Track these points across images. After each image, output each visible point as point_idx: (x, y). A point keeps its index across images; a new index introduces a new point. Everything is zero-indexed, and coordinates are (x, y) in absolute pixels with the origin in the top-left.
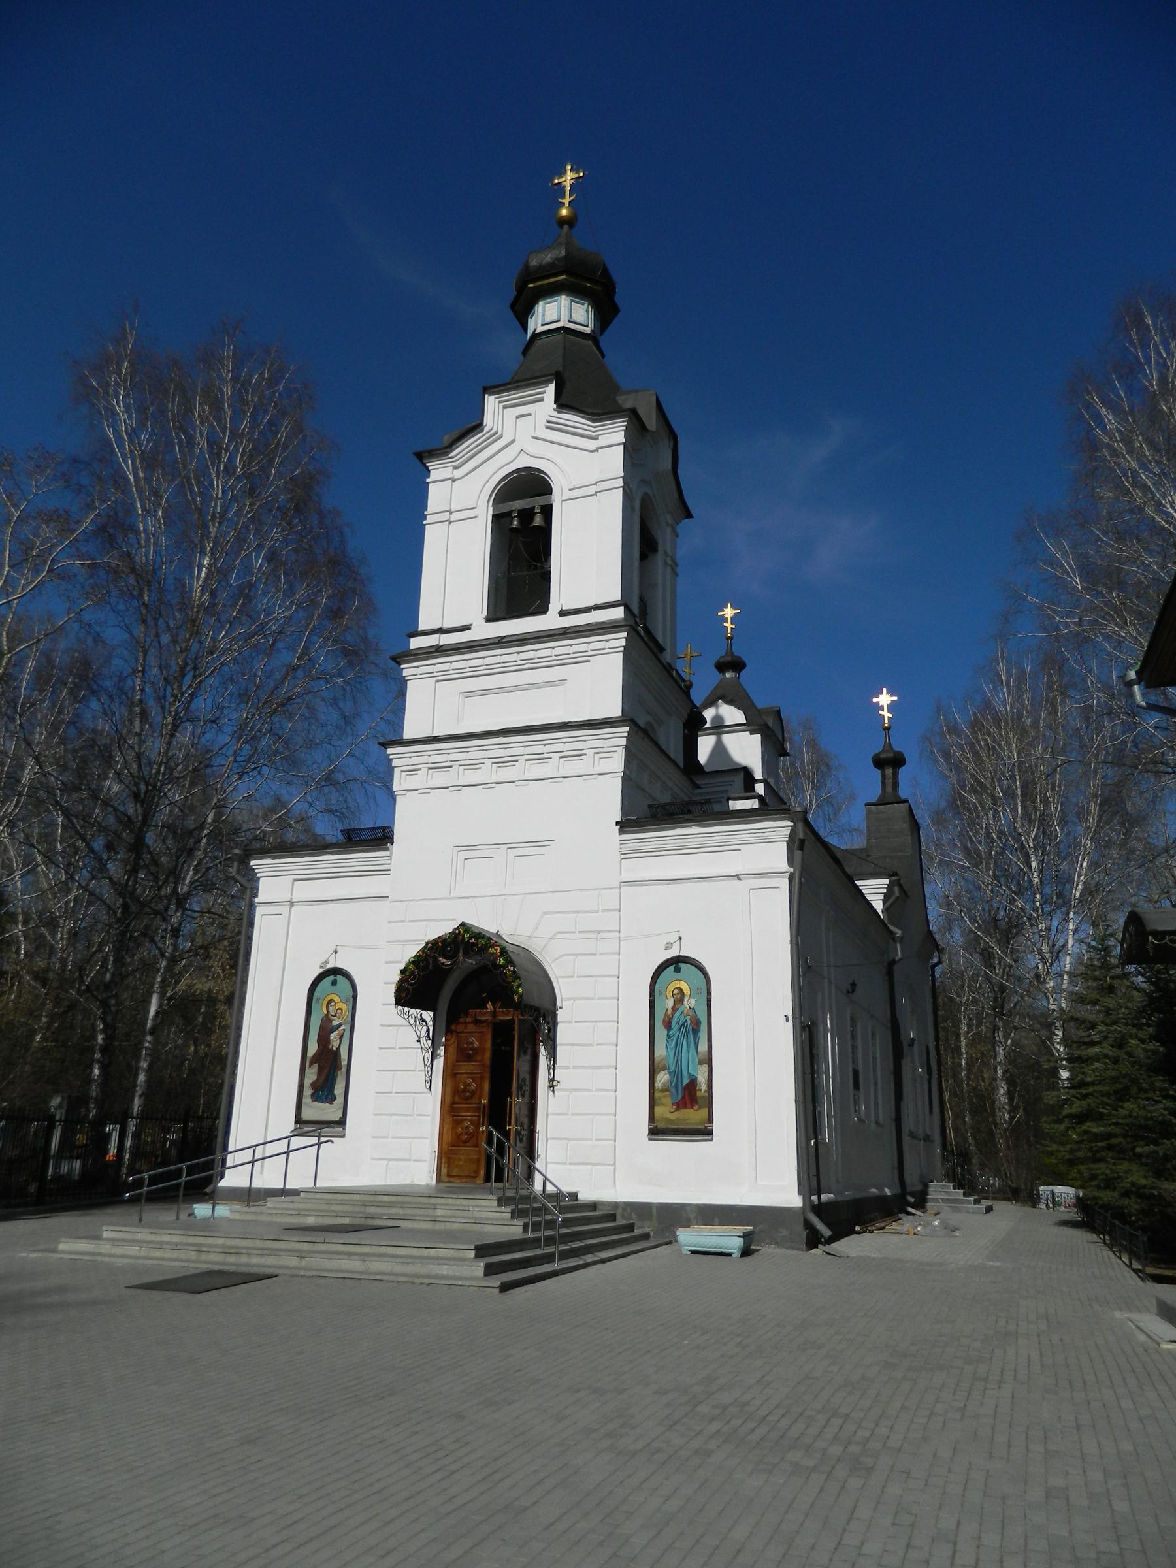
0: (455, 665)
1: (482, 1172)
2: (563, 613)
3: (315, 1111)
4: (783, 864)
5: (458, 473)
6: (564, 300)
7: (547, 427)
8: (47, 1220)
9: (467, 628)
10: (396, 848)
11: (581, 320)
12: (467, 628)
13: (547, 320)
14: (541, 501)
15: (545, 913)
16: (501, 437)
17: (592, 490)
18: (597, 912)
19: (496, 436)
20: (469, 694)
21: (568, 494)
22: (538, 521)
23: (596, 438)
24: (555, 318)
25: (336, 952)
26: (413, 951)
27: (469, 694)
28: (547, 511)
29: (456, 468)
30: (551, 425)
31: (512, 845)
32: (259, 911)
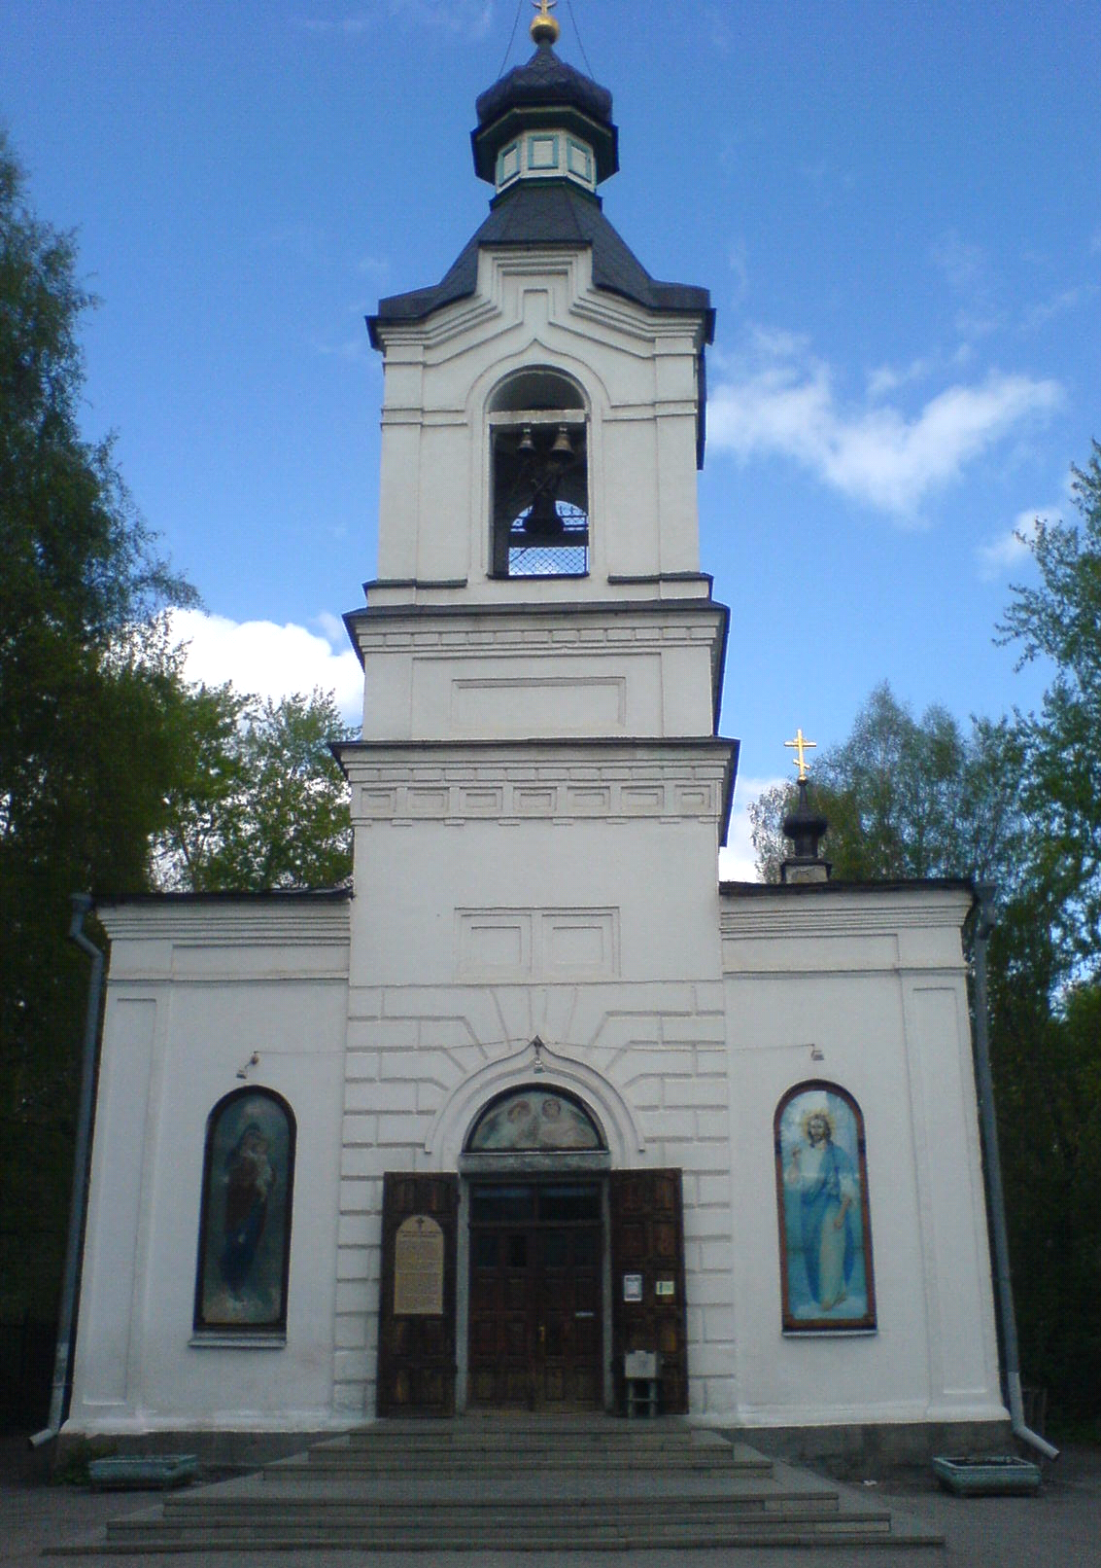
0: (446, 639)
1: (727, 1346)
3: (232, 1307)
4: (958, 959)
5: (432, 357)
6: (562, 137)
7: (572, 313)
8: (255, 1359)
9: (461, 585)
10: (357, 908)
11: (582, 171)
12: (461, 585)
13: (538, 163)
14: (571, 416)
15: (611, 1014)
16: (499, 315)
17: (649, 413)
18: (688, 1014)
19: (493, 314)
20: (465, 684)
21: (610, 414)
22: (562, 444)
23: (652, 340)
24: (549, 162)
25: (254, 1062)
26: (221, 1096)
27: (465, 684)
28: (578, 434)
29: (427, 348)
30: (578, 312)
31: (550, 912)
32: (112, 994)
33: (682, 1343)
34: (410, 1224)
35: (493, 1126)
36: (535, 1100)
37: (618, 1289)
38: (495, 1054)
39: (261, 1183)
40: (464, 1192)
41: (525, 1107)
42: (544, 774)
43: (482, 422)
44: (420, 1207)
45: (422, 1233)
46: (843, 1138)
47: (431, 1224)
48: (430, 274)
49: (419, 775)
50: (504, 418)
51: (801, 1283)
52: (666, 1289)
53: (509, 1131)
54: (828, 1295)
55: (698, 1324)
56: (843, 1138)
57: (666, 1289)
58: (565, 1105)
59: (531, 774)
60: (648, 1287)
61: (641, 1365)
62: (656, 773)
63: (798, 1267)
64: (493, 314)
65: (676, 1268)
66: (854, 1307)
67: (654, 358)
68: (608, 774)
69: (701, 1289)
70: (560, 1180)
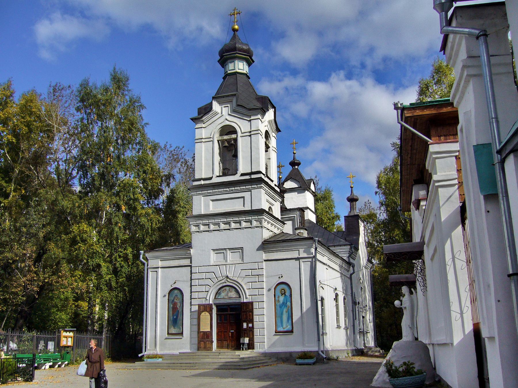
2: (242, 175)
3: (173, 331)
14: (234, 136)
24: (233, 68)
28: (236, 140)
31: (230, 249)
33: (253, 336)
34: (203, 314)
35: (220, 294)
36: (227, 288)
37: (99, 345)
38: (219, 279)
39: (178, 307)
40: (214, 308)
41: (225, 289)
42: (228, 220)
43: (217, 137)
44: (205, 310)
45: (205, 315)
46: (288, 294)
47: (207, 314)
48: (245, 76)
49: (204, 222)
50: (220, 138)
51: (279, 324)
52: (250, 325)
53: (223, 295)
54: (284, 326)
55: (256, 332)
56: (288, 294)
57: (250, 325)
58: (233, 290)
59: (226, 220)
60: (247, 325)
61: (246, 340)
62: (251, 218)
63: (279, 320)
64: (217, 114)
65: (252, 321)
66: (289, 328)
67: (250, 120)
68: (240, 219)
69: (257, 324)
70: (512, 252)
